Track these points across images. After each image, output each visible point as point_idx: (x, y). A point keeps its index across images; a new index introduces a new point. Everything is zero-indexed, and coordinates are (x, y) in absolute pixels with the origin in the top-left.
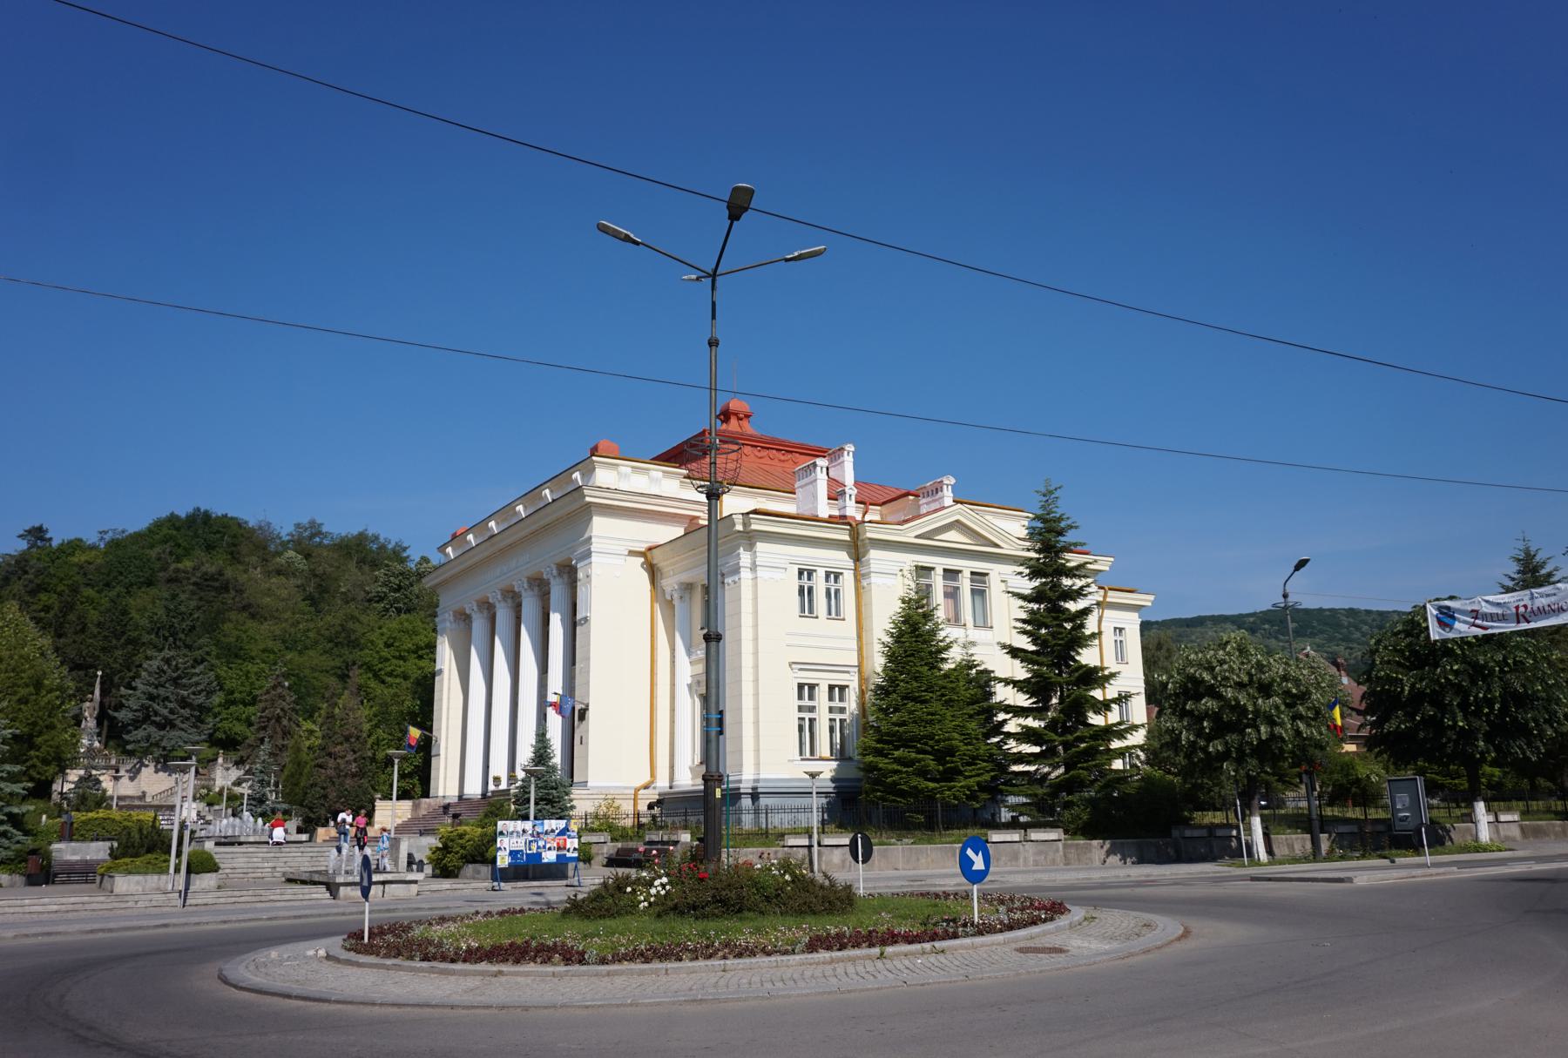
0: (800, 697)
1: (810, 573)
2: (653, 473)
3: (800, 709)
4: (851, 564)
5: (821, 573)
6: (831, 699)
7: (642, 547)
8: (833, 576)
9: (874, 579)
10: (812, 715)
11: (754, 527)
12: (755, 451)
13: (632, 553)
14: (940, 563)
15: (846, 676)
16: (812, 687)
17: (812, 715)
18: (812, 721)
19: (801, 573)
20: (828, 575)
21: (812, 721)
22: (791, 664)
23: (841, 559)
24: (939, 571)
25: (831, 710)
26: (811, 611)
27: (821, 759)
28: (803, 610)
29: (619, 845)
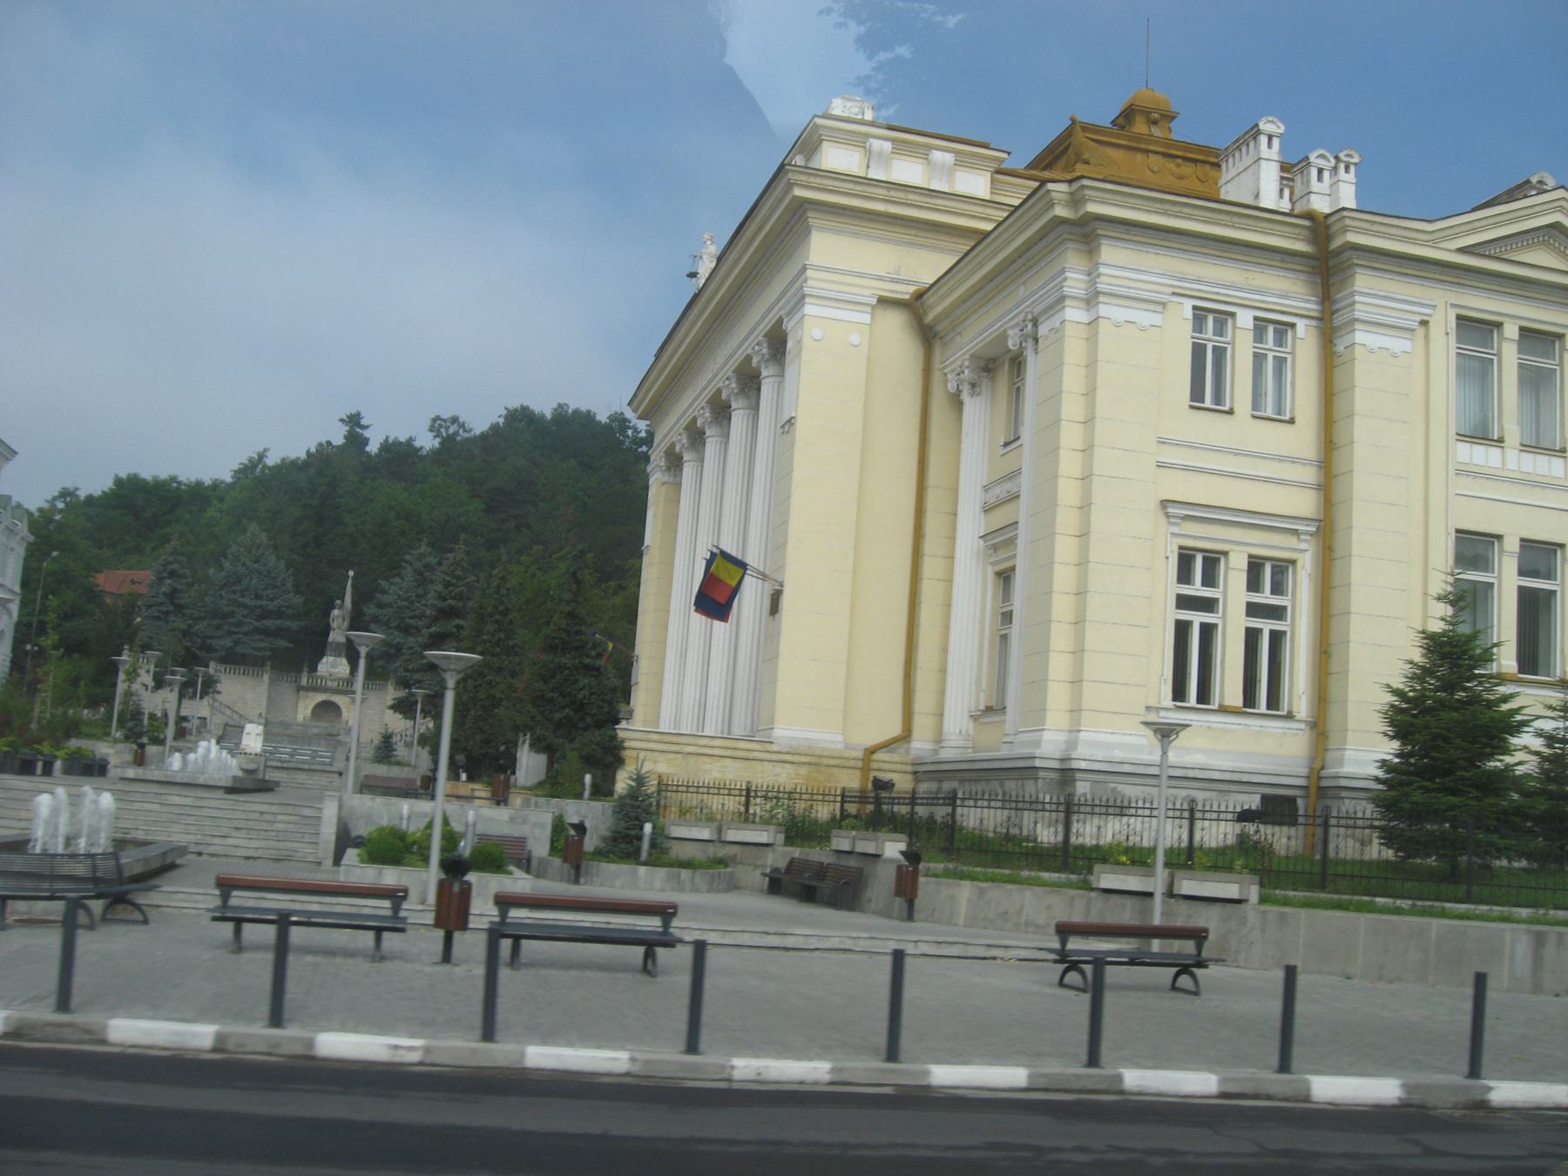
0: (1184, 575)
1: (1223, 319)
2: (937, 156)
3: (1184, 602)
4: (1312, 307)
5: (1245, 319)
6: (1254, 584)
7: (905, 292)
8: (1273, 328)
9: (1361, 336)
10: (1277, 626)
11: (1092, 208)
12: (1171, 165)
13: (884, 302)
14: (1515, 313)
15: (1292, 541)
16: (1212, 562)
17: (1277, 626)
18: (1277, 638)
19: (1199, 315)
20: (1260, 325)
21: (1277, 638)
22: (1165, 503)
23: (1288, 293)
24: (1511, 331)
25: (1253, 610)
26: (1218, 399)
27: (1224, 710)
28: (1197, 393)
29: (796, 852)
